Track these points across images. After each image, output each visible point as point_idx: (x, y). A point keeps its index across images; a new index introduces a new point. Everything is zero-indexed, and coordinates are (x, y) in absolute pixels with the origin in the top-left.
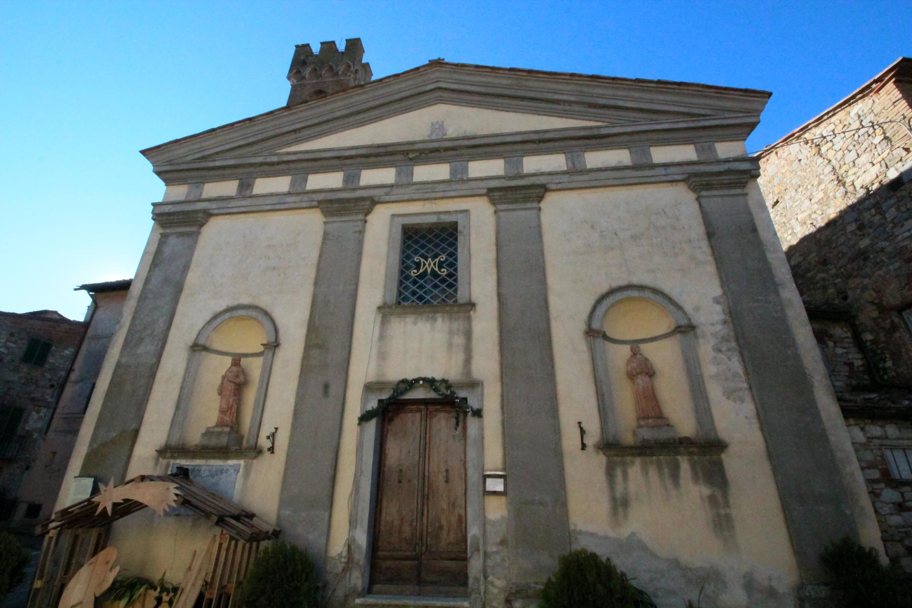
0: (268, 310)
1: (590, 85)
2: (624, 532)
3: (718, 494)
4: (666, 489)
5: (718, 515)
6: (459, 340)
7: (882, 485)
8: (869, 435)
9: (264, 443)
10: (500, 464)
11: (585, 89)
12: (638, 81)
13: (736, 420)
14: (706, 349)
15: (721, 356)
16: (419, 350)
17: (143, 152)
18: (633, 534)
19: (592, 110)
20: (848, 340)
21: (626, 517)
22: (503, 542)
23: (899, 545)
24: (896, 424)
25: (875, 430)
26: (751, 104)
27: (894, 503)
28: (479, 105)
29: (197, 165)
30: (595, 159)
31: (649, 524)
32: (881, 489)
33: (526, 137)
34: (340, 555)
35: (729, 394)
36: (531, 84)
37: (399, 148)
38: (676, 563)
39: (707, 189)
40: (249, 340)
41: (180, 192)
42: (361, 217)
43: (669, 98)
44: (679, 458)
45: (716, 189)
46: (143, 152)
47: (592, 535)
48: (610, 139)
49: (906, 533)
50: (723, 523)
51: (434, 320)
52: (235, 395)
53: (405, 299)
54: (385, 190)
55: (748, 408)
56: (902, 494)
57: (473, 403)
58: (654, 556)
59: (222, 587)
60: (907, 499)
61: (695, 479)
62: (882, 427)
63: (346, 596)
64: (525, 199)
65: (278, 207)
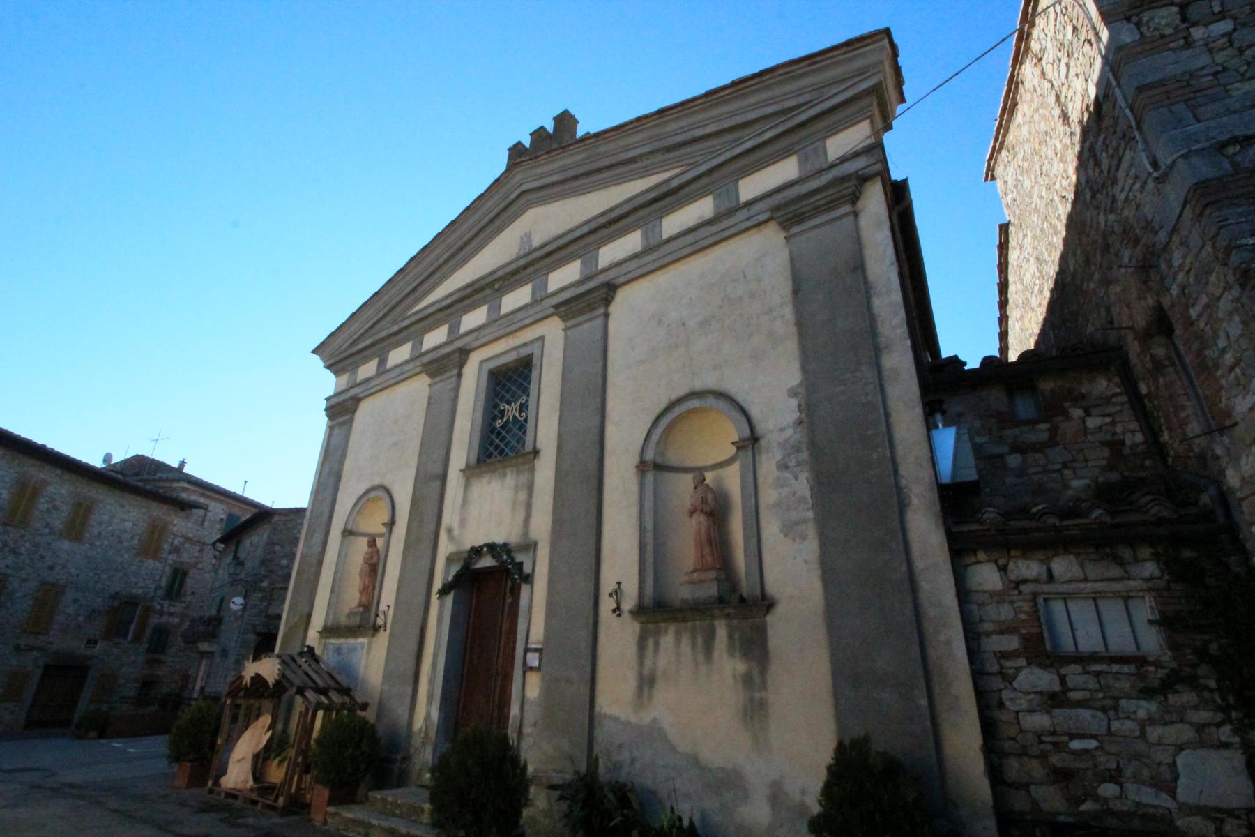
0: (390, 487)
1: (658, 125)
2: (646, 717)
3: (755, 672)
4: (697, 665)
5: (752, 700)
6: (522, 496)
7: (1022, 662)
8: (1013, 577)
9: (380, 621)
10: (541, 638)
11: (657, 131)
12: (709, 94)
13: (790, 565)
14: (768, 467)
15: (787, 475)
16: (485, 513)
17: (314, 352)
18: (655, 720)
19: (671, 155)
20: (1120, 399)
21: (650, 697)
22: (535, 724)
23: (1035, 764)
24: (1077, 555)
25: (1028, 568)
26: (877, 53)
27: (1041, 693)
28: (562, 196)
29: (350, 352)
30: (674, 223)
31: (673, 710)
32: (1018, 669)
33: (593, 225)
34: (420, 730)
35: (789, 529)
36: (602, 149)
37: (483, 282)
38: (695, 760)
39: (800, 222)
40: (374, 522)
41: (345, 378)
42: (602, 310)
43: (752, 100)
44: (717, 623)
45: (810, 218)
46: (314, 352)
47: (616, 719)
48: (686, 190)
49: (1055, 744)
50: (755, 711)
51: (504, 475)
52: (370, 575)
53: (490, 456)
54: (475, 334)
55: (811, 547)
56: (1062, 679)
57: (527, 569)
58: (673, 748)
59: (691, 820)
60: (1070, 685)
61: (731, 650)
62: (1046, 562)
63: (421, 770)
64: (591, 308)
65: (401, 378)
